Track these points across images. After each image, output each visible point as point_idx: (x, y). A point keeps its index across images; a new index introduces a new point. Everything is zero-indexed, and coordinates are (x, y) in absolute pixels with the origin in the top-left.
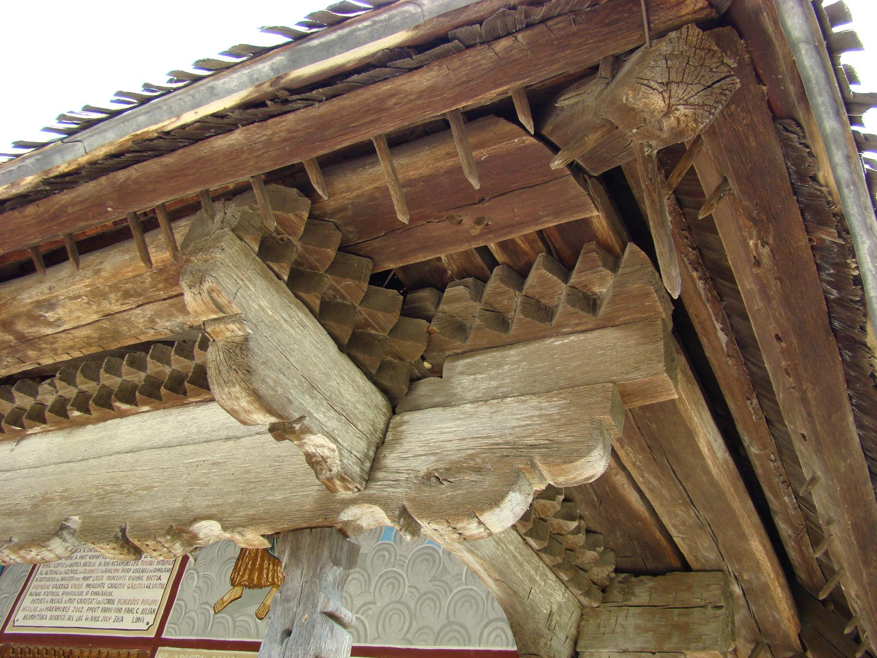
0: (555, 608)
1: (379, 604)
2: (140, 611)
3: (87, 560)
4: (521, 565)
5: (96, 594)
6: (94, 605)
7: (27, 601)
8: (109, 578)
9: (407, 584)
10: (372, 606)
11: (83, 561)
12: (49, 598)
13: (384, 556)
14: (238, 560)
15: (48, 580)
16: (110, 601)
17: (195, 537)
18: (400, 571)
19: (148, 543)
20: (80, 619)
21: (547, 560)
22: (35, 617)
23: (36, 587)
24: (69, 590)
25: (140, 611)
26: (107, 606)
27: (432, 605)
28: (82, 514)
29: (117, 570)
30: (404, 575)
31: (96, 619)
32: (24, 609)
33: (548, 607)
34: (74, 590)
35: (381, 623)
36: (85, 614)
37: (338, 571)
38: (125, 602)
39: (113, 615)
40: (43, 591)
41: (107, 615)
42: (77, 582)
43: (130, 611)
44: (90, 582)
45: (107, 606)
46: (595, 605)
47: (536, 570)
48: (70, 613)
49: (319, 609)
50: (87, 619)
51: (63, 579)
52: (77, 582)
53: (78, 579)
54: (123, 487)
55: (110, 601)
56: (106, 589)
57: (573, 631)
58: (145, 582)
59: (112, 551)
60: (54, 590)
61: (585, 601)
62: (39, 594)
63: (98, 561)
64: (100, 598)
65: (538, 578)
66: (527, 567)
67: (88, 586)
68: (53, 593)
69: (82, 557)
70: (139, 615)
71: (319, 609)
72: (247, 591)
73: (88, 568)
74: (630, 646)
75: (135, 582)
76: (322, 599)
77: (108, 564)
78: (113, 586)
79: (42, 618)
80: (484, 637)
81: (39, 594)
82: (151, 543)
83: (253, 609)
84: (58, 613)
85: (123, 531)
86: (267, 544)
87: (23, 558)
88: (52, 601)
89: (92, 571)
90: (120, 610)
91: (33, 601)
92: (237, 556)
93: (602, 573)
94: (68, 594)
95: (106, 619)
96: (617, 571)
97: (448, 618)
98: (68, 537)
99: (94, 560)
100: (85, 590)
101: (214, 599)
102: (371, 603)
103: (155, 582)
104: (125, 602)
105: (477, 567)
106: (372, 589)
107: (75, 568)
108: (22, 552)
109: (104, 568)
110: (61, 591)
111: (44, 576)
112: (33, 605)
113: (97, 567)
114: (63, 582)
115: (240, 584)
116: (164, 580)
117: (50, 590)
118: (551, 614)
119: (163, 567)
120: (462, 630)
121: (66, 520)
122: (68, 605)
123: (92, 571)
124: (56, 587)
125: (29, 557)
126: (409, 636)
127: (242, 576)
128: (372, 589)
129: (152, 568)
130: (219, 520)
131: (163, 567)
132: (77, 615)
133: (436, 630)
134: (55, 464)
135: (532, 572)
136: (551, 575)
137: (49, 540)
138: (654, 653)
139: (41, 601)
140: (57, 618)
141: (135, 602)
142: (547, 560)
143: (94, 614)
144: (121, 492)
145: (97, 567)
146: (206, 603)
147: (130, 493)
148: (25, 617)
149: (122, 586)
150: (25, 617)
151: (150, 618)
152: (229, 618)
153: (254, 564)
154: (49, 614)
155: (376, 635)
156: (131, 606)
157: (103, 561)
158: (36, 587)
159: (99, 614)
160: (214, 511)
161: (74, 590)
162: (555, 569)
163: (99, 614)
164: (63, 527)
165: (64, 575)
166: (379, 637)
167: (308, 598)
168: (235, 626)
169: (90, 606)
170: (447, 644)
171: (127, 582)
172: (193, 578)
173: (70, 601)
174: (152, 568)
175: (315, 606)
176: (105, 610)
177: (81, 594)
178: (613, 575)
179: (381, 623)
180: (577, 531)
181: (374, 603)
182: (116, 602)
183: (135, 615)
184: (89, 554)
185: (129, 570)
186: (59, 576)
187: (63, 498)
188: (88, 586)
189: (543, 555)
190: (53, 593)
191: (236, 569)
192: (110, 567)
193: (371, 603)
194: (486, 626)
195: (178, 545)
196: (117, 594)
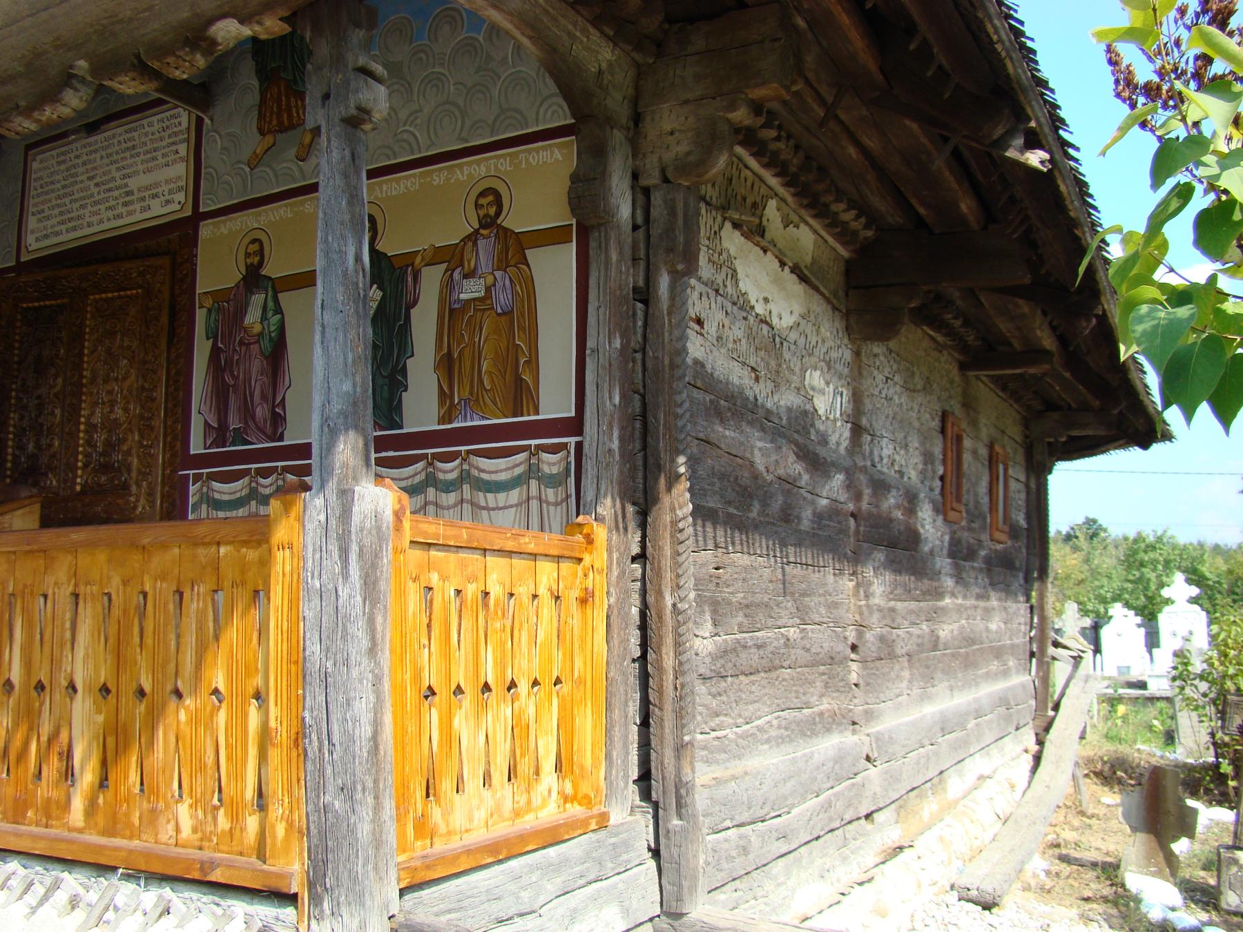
0: (604, 66)
1: (426, 111)
2: (166, 193)
3: (85, 158)
4: (555, 20)
5: (110, 190)
6: (112, 203)
7: (32, 222)
8: (118, 169)
9: (452, 82)
10: (419, 114)
11: (80, 161)
12: (56, 211)
13: (421, 59)
14: (260, 107)
15: (47, 193)
16: (128, 194)
17: (214, 43)
18: (441, 70)
19: (168, 60)
20: (101, 222)
21: (584, 13)
22: (47, 232)
23: (35, 205)
24: (77, 196)
25: (166, 193)
26: (127, 199)
27: (481, 96)
28: (86, 57)
29: (124, 159)
30: (447, 73)
31: (120, 216)
32: (33, 232)
33: (596, 65)
34: (81, 194)
35: (432, 132)
36: (105, 215)
37: (361, 34)
38: (147, 189)
39: (137, 206)
40: (46, 207)
41: (131, 208)
42: (82, 186)
43: (155, 196)
44: (98, 180)
45: (127, 199)
46: (651, 61)
47: (575, 24)
48: (88, 219)
49: (350, 66)
50: (109, 220)
51: (64, 187)
52: (82, 186)
53: (82, 182)
54: (121, 16)
55: (128, 194)
56: (119, 182)
57: (631, 91)
58: (161, 161)
59: (133, 83)
60: (59, 201)
61: (638, 57)
62: (43, 211)
63: (98, 156)
64: (116, 193)
65: (578, 34)
66: (563, 21)
67: (97, 185)
68: (59, 206)
69: (77, 157)
70: (168, 197)
71: (350, 66)
72: (279, 136)
73: (89, 166)
74: (690, 96)
75: (151, 164)
76: (350, 58)
77: (111, 155)
78: (125, 177)
79: (57, 234)
80: (541, 116)
81: (43, 211)
82: (170, 60)
83: (293, 151)
84: (71, 225)
85: (138, 56)
86: (287, 29)
87: (38, 121)
88: (61, 214)
89: (95, 168)
90: (143, 199)
91: (40, 221)
92: (257, 102)
93: (652, 24)
94: (76, 200)
95: (130, 213)
96: (669, 20)
97: (501, 107)
98: (79, 86)
99: (94, 156)
100: (95, 191)
101: (246, 154)
102: (417, 111)
103: (173, 157)
104: (147, 189)
105: (507, 25)
106: (415, 98)
107: (73, 171)
108: (36, 114)
109: (108, 161)
110: (67, 200)
111: (40, 190)
112: (41, 225)
113: (99, 162)
114: (66, 190)
115: (270, 132)
116: (183, 152)
117: (54, 202)
118: (600, 72)
119: (177, 139)
120: (517, 116)
121: (71, 67)
122: (82, 212)
123: (95, 168)
124: (59, 198)
125: (44, 119)
126: (464, 134)
127: (270, 122)
128: (415, 98)
129: (164, 143)
130: (234, 16)
131: (177, 139)
132: (95, 219)
133: (490, 122)
134: (32, 15)
135: (570, 27)
136: (592, 30)
137: (60, 92)
138: (714, 98)
139: (48, 218)
140: (74, 229)
141: (157, 185)
142: (584, 13)
143: (115, 212)
144: (121, 22)
145: (99, 162)
146: (239, 162)
147: (131, 20)
148: (37, 240)
149: (136, 173)
150: (37, 240)
151: (181, 197)
152: (267, 170)
153: (279, 106)
154: (63, 227)
155: (429, 142)
156: (154, 191)
157: (104, 153)
158: (35, 205)
159: (121, 210)
160: (226, 9)
161: (81, 194)
162: (596, 22)
163: (121, 210)
164: (71, 76)
165: (64, 183)
166: (433, 144)
167: (338, 61)
168: (276, 176)
169: (107, 205)
170: (504, 133)
171: (141, 167)
172: (215, 141)
173: (83, 207)
174: (164, 143)
175: (346, 66)
176: (126, 204)
177: (92, 196)
178: (666, 26)
179: (432, 132)
180: (778, 139)
181: (421, 110)
182: (136, 192)
183: (163, 199)
184: (85, 150)
185: (138, 155)
186: (58, 186)
187: (57, 48)
188: (97, 185)
189: (579, 7)
190: (59, 206)
191: (261, 117)
192: (115, 157)
193: (417, 111)
194: (541, 105)
195: (198, 56)
196: (133, 183)
